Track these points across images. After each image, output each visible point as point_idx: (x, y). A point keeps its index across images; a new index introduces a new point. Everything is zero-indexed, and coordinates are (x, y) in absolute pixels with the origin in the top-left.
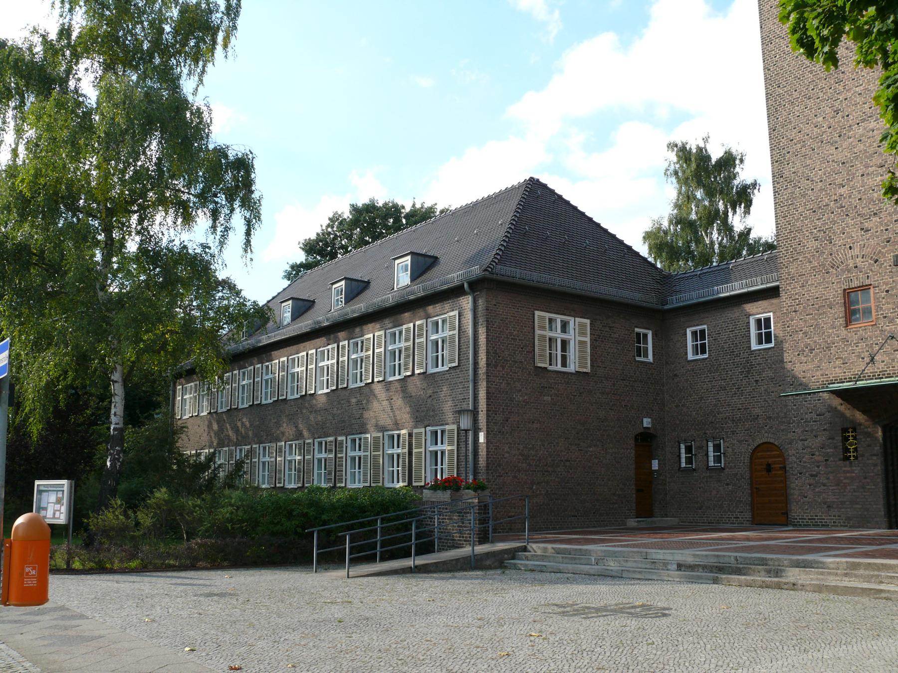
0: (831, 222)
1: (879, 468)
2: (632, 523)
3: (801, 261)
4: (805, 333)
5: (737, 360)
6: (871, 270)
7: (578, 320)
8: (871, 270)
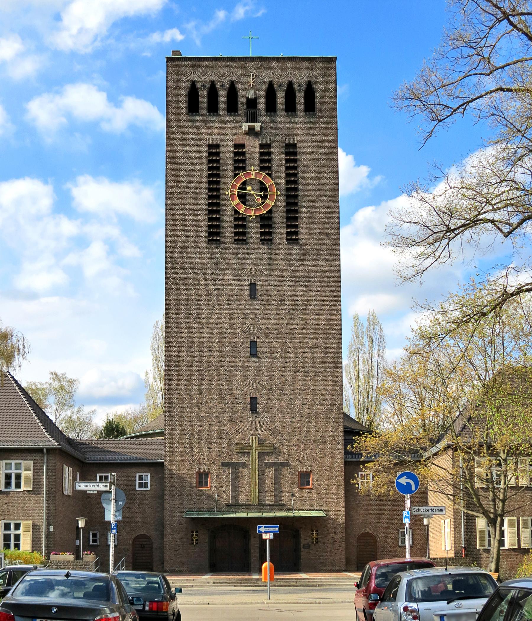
4: (176, 488)
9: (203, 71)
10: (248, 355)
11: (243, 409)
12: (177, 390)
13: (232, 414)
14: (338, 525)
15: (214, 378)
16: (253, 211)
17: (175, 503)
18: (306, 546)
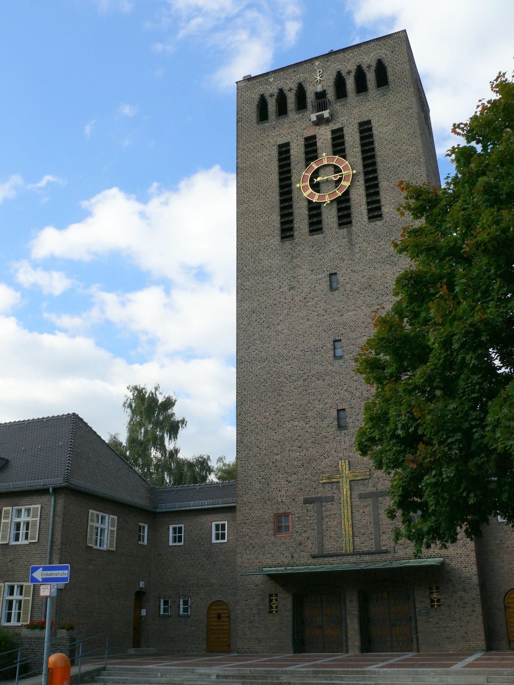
0: (269, 474)
1: (290, 618)
2: (132, 651)
3: (250, 494)
4: (250, 537)
5: (202, 548)
6: (291, 505)
7: (111, 516)
8: (291, 505)
11: (328, 426)
12: (250, 412)
16: (327, 197)
18: (424, 611)
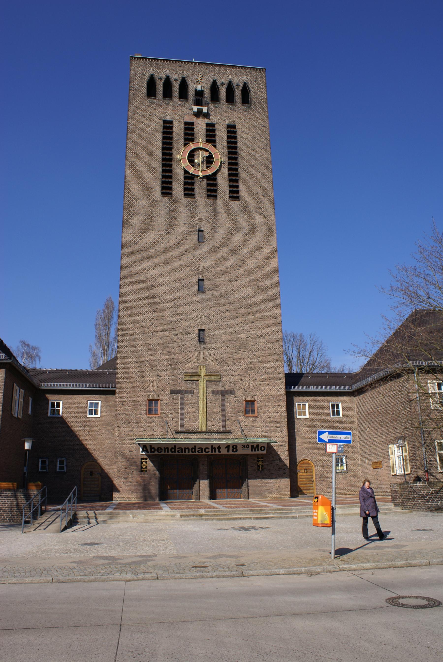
4: (127, 415)
9: (161, 69)
10: (196, 292)
12: (130, 320)
13: (181, 344)
14: (282, 452)
15: (165, 311)
17: (125, 430)
